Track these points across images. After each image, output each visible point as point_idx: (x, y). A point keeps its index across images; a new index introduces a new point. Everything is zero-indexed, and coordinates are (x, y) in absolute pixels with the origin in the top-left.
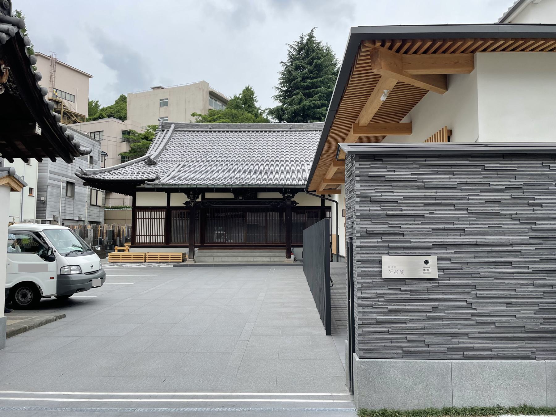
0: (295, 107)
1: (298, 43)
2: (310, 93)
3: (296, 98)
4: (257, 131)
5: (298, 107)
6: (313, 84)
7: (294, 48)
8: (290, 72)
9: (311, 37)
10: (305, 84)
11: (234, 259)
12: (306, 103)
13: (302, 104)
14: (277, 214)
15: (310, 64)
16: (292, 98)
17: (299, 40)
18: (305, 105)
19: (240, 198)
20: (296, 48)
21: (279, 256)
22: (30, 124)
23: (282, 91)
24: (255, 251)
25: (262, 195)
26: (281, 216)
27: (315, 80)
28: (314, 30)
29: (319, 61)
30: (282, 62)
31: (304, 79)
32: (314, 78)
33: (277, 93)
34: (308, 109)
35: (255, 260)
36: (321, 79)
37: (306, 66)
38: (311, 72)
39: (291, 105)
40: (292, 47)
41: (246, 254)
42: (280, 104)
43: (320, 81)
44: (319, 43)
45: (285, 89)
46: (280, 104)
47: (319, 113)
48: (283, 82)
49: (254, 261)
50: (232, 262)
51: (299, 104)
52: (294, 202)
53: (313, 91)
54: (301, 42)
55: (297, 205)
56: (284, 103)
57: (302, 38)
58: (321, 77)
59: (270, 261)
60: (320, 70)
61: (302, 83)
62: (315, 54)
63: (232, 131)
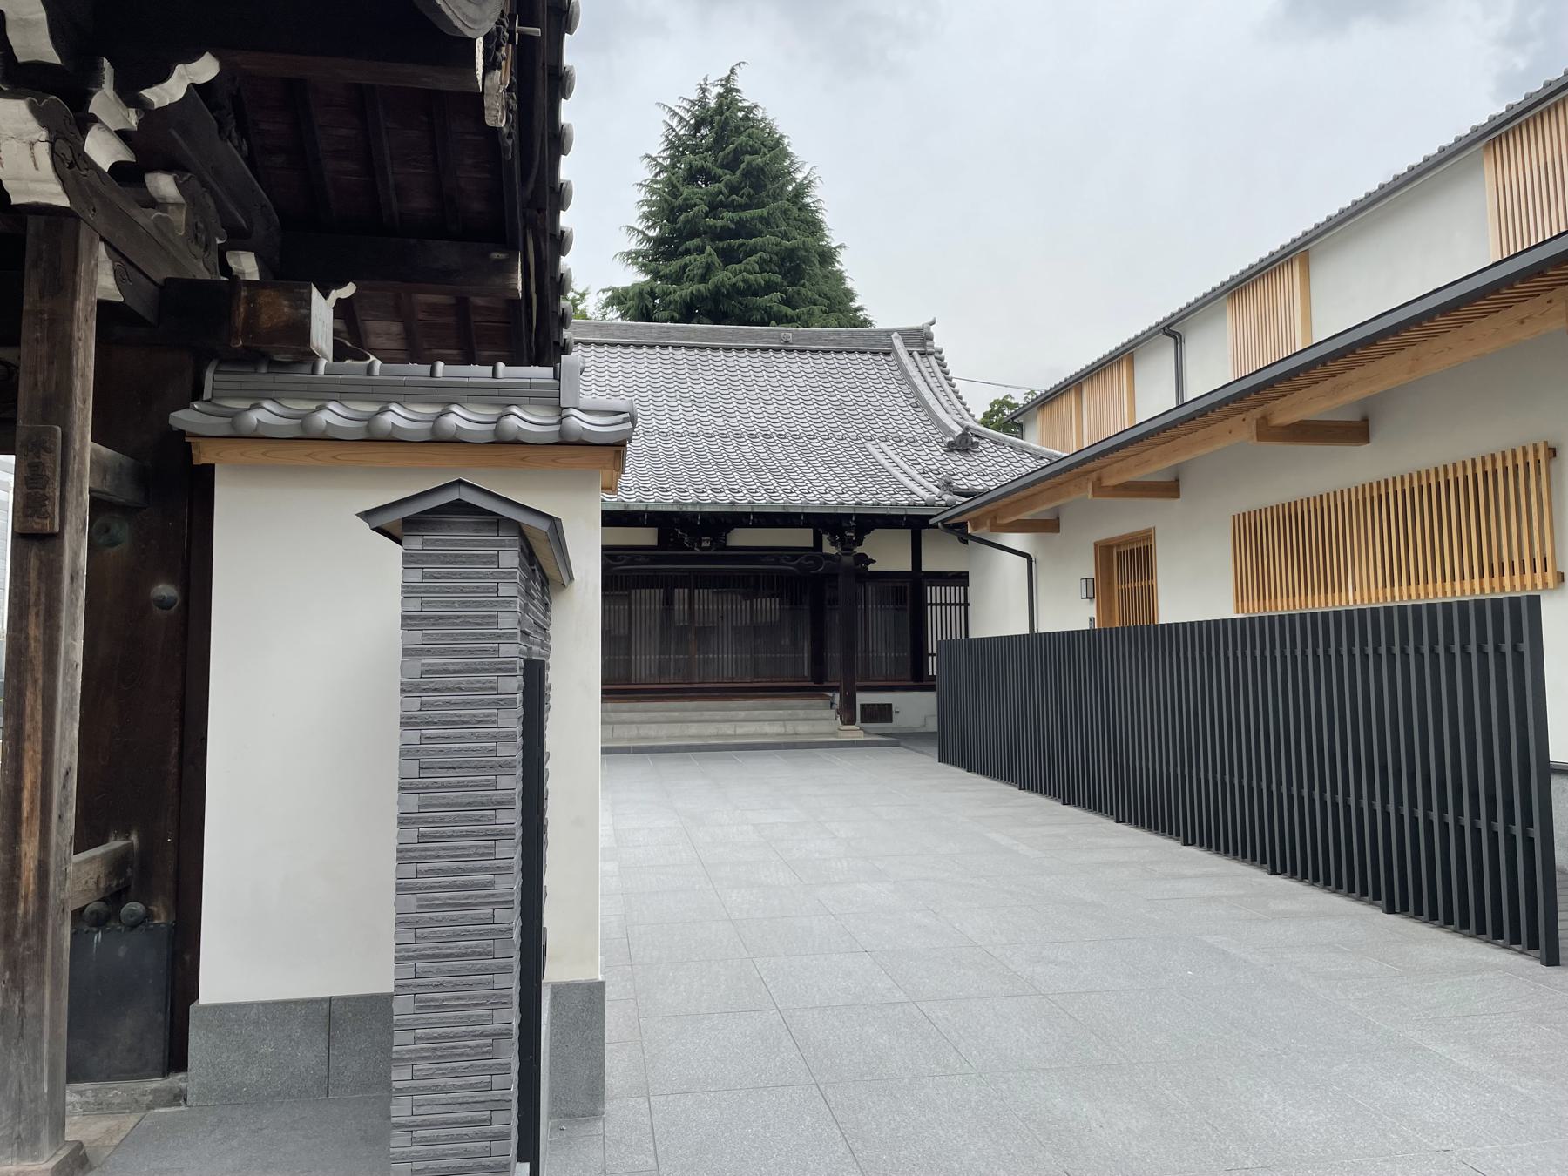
0: (694, 288)
1: (693, 103)
2: (731, 249)
3: (696, 262)
4: (690, 348)
5: (702, 287)
6: (740, 223)
7: (682, 119)
8: (674, 186)
9: (729, 90)
10: (720, 223)
11: (676, 729)
12: (725, 276)
13: (713, 280)
14: (658, 593)
15: (732, 164)
16: (681, 262)
17: (694, 96)
18: (723, 284)
19: (706, 544)
20: (687, 116)
21: (818, 718)
22: (495, 255)
23: (649, 239)
24: (641, 705)
25: (740, 538)
26: (668, 601)
27: (747, 214)
28: (737, 70)
29: (758, 160)
30: (648, 156)
31: (714, 208)
32: (744, 207)
33: (633, 244)
34: (729, 296)
35: (739, 731)
36: (764, 212)
37: (720, 171)
38: (734, 189)
39: (676, 278)
40: (676, 114)
41: (707, 715)
42: (642, 278)
43: (761, 218)
44: (750, 109)
45: (652, 233)
46: (642, 278)
47: (758, 308)
48: (650, 213)
49: (735, 736)
50: (669, 738)
51: (703, 279)
52: (864, 559)
53: (741, 245)
54: (702, 103)
55: (871, 567)
56: (656, 275)
57: (704, 91)
58: (762, 205)
59: (785, 735)
60: (758, 187)
61: (710, 221)
62: (743, 138)
63: (613, 345)
